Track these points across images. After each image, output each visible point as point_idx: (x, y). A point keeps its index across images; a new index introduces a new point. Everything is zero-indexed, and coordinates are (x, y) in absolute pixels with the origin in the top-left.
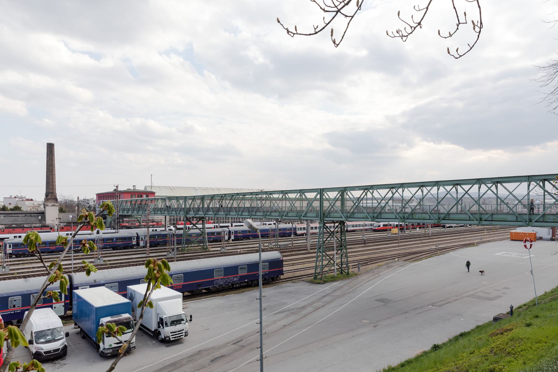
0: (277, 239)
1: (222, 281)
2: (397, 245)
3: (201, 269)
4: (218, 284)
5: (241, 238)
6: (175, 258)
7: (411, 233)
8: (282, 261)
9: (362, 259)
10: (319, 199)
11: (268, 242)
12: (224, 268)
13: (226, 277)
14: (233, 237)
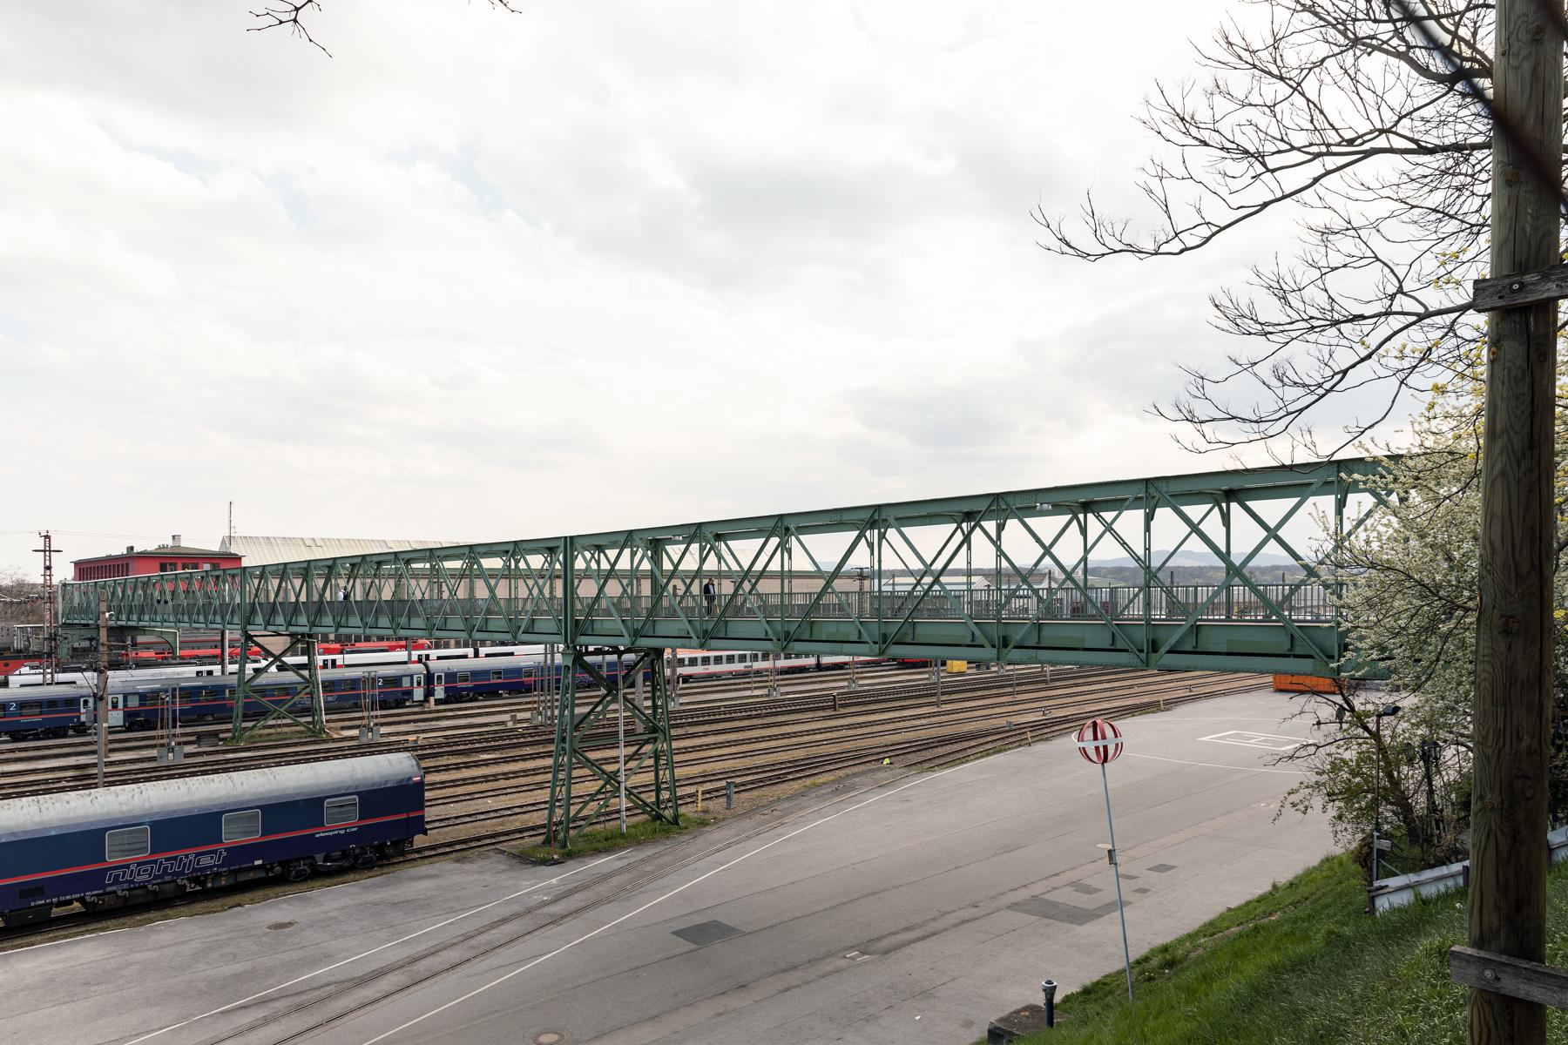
0: (549, 698)
1: (144, 871)
2: (936, 709)
3: (39, 830)
4: (127, 881)
5: (468, 695)
6: (101, 775)
7: (1002, 672)
8: (420, 787)
9: (781, 763)
10: (562, 573)
11: (530, 706)
12: (154, 825)
13: (161, 857)
14: (440, 693)
